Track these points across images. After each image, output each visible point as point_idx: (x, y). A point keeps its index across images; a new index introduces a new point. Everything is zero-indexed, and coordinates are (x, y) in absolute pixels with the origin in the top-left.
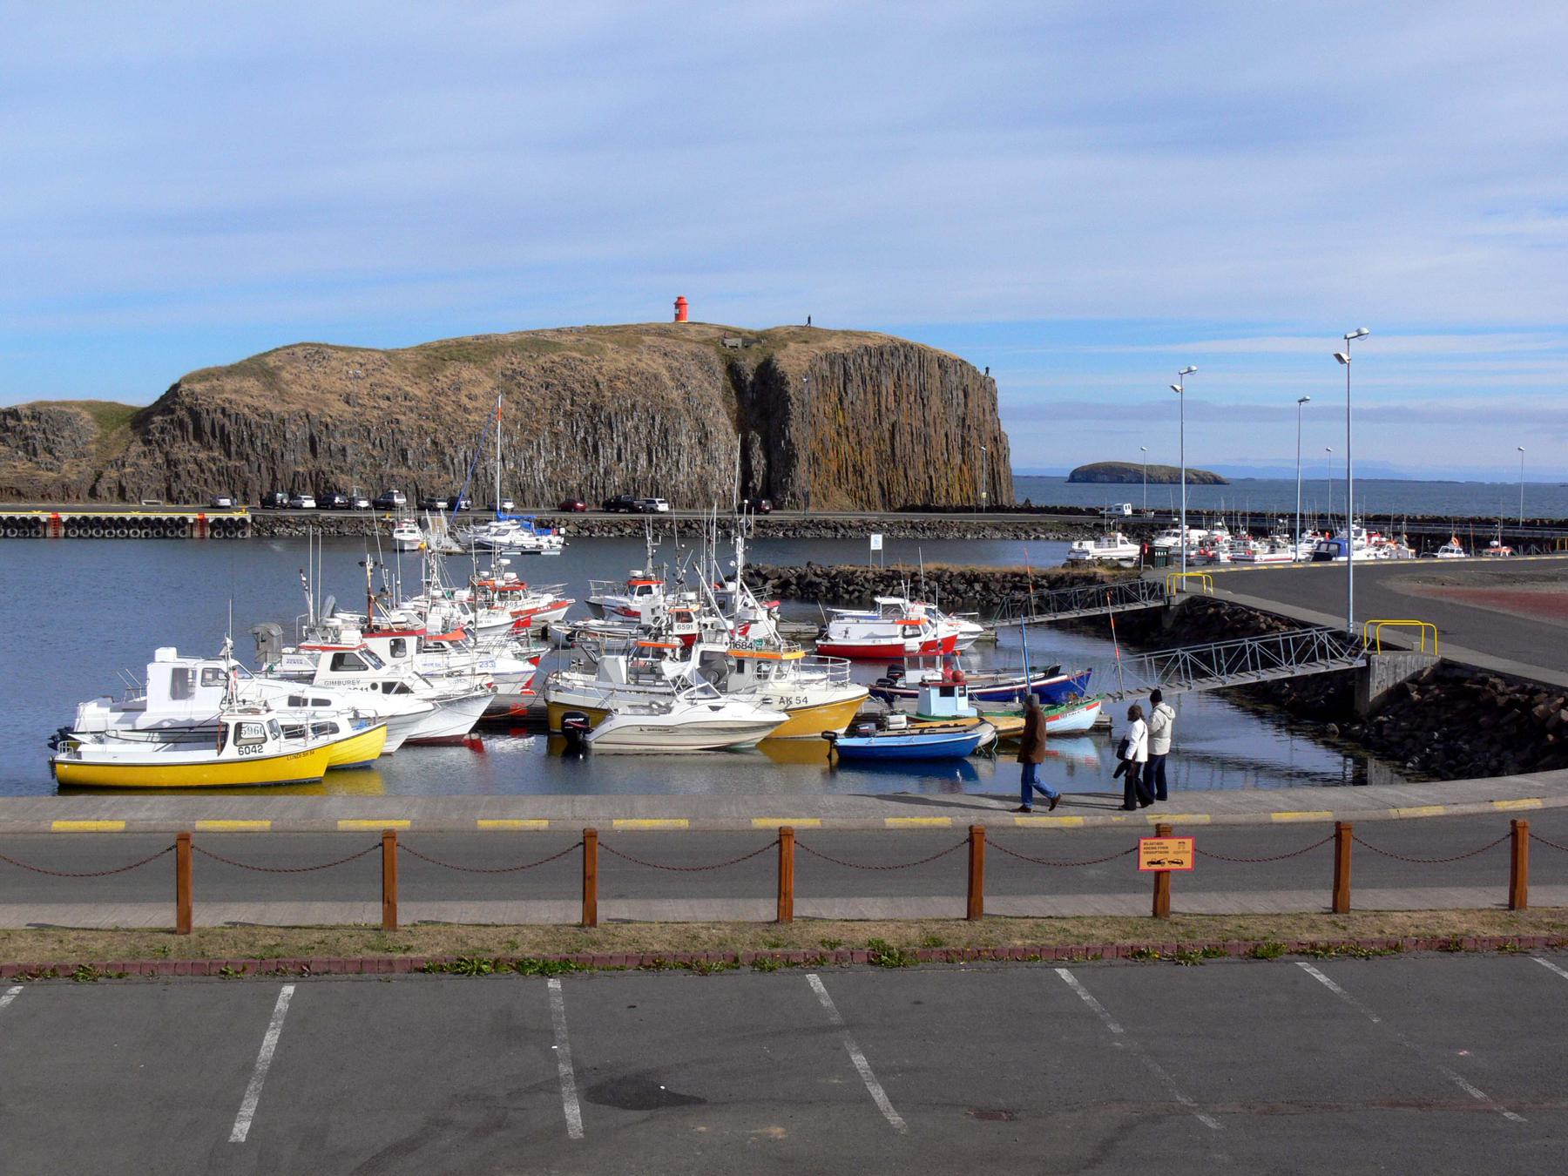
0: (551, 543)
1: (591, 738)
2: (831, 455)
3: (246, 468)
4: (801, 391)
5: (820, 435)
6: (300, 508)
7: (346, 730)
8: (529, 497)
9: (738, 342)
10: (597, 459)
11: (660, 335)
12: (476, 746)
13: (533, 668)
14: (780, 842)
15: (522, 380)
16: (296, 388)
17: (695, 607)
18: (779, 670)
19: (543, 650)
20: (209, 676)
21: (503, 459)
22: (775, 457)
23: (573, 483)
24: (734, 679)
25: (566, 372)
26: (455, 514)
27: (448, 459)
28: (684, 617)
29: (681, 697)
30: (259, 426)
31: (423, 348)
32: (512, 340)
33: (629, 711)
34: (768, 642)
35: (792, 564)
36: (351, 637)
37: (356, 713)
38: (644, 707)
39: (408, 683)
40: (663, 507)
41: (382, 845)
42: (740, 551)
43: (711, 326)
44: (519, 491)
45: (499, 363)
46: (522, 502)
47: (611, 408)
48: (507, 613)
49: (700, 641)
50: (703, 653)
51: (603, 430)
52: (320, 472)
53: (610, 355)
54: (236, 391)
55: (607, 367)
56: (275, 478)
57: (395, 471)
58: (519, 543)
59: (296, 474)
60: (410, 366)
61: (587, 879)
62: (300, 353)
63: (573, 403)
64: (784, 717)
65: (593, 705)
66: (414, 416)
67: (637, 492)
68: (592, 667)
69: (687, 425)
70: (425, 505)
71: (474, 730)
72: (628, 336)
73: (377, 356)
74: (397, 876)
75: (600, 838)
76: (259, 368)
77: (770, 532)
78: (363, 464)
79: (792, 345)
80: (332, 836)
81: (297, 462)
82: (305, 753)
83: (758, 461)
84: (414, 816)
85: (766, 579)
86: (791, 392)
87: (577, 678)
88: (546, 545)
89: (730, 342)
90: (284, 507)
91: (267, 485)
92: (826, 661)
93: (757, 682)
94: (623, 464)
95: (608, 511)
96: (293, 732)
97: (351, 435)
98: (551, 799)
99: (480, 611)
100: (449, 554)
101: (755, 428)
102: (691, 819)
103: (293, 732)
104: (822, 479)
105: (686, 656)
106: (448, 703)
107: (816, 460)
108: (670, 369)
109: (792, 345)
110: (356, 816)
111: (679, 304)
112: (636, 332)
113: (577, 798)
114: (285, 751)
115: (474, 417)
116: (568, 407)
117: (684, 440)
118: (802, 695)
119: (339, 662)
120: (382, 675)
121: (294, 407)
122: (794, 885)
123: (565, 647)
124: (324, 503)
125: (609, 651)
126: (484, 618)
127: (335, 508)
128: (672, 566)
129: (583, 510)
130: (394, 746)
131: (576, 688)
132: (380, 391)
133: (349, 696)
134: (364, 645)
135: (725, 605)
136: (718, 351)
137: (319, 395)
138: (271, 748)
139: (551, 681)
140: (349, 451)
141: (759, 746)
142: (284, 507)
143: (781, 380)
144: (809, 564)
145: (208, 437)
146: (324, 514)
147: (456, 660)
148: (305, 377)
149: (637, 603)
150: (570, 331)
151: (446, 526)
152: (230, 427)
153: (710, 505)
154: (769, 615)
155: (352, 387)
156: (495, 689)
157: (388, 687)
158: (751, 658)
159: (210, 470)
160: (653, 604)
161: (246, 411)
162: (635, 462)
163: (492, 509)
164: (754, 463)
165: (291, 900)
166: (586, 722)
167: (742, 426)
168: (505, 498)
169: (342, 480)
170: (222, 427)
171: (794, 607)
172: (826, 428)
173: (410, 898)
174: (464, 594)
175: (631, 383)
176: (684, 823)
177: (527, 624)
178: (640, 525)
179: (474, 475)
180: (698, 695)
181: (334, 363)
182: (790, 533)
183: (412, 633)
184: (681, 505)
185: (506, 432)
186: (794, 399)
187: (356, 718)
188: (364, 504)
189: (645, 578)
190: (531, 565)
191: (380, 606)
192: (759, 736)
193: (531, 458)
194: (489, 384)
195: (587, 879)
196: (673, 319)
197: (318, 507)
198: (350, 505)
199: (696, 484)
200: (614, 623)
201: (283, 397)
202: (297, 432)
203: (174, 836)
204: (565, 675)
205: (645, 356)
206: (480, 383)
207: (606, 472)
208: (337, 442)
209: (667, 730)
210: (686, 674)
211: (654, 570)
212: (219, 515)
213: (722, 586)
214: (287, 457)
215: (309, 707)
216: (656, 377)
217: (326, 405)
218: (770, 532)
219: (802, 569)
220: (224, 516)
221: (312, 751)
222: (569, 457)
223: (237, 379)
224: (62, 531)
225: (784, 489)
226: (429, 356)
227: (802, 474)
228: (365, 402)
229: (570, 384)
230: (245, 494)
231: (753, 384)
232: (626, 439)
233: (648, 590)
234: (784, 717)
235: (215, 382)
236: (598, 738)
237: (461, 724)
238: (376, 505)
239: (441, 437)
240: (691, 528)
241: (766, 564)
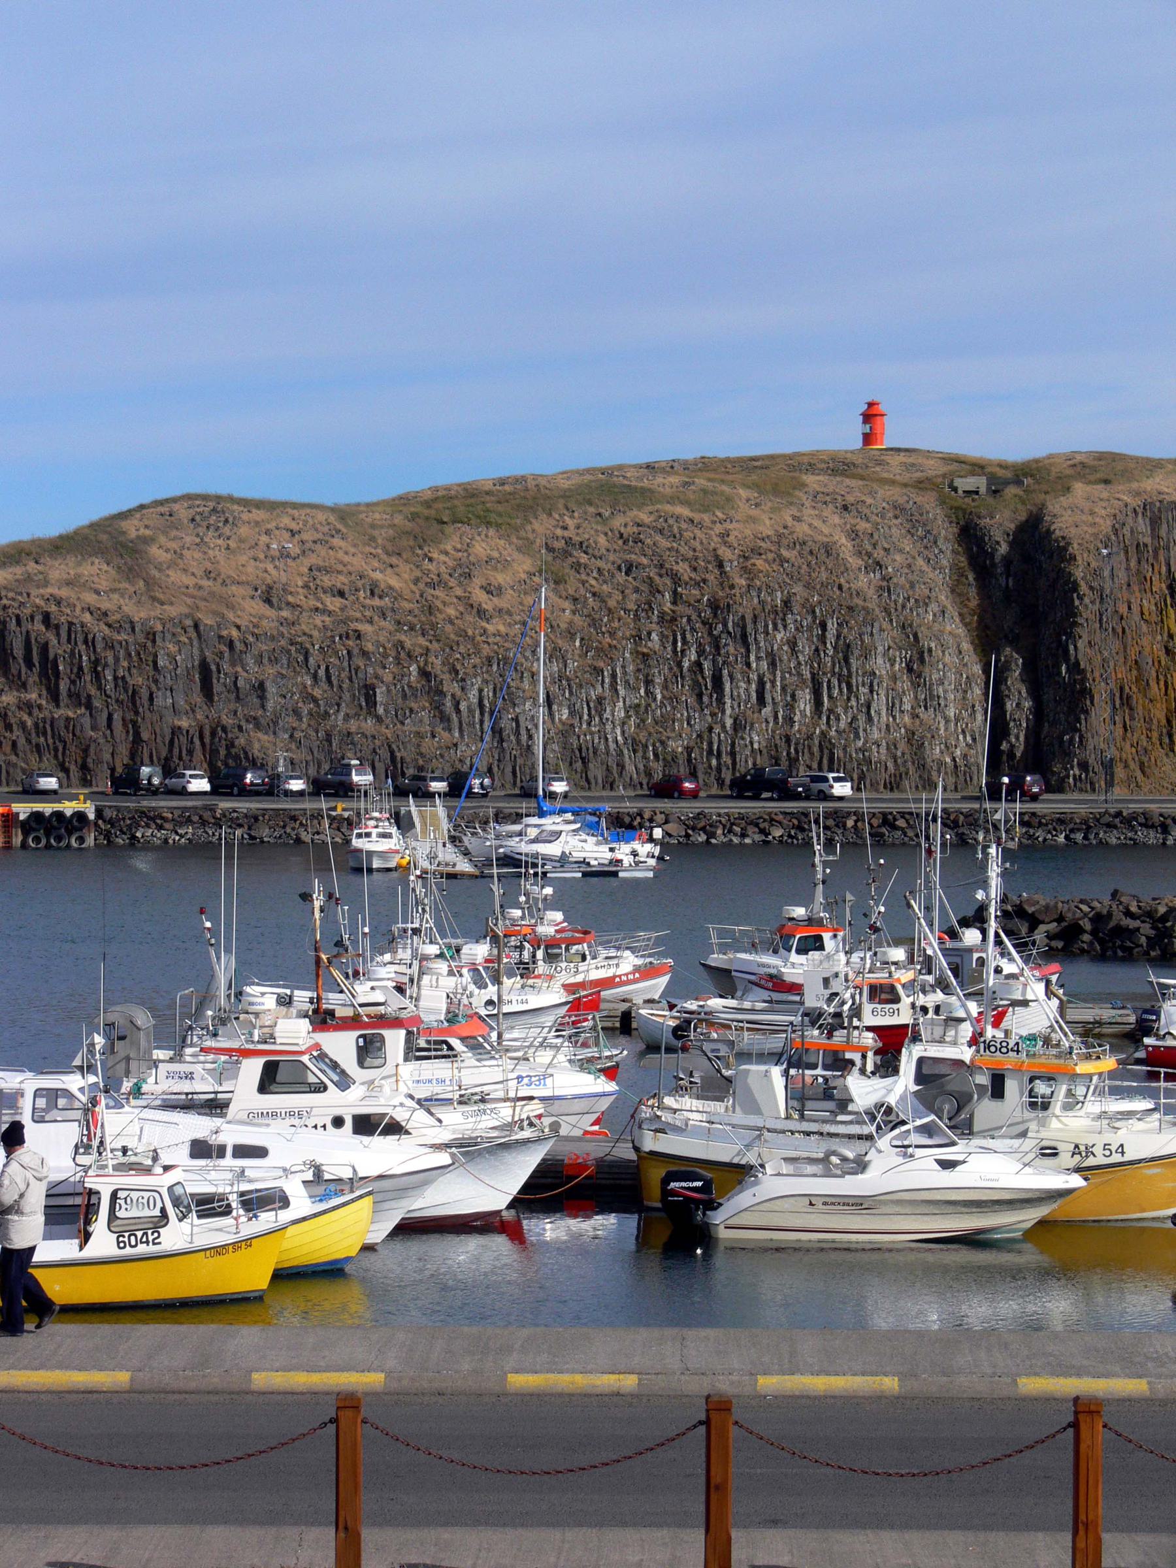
0: (637, 855)
1: (718, 1218)
2: (1155, 690)
3: (87, 721)
4: (1097, 573)
5: (1133, 654)
6: (183, 792)
7: (301, 1203)
8: (596, 771)
9: (979, 483)
10: (721, 701)
11: (834, 472)
12: (514, 1231)
13: (611, 1087)
14: (1075, 1425)
15: (584, 559)
16: (175, 577)
17: (905, 976)
18: (1070, 1094)
19: (617, 1052)
20: (41, 1103)
21: (549, 702)
22: (1049, 695)
23: (677, 746)
24: (985, 1111)
25: (664, 543)
26: (462, 802)
27: (448, 703)
28: (885, 994)
29: (884, 1142)
30: (110, 645)
31: (403, 500)
32: (565, 484)
33: (785, 1168)
34: (1047, 1041)
35: (1087, 891)
36: (294, 1032)
37: (318, 1170)
38: (812, 1161)
39: (400, 1116)
40: (842, 789)
41: (335, 1421)
42: (994, 872)
43: (928, 454)
44: (578, 759)
45: (542, 526)
46: (582, 781)
47: (746, 606)
48: (557, 985)
49: (916, 1038)
50: (921, 1061)
51: (731, 648)
52: (218, 728)
53: (744, 510)
54: (69, 583)
55: (740, 531)
56: (137, 739)
57: (353, 725)
58: (578, 855)
59: (176, 731)
60: (381, 535)
61: (715, 1492)
62: (183, 512)
63: (676, 598)
64: (1076, 1181)
65: (725, 1158)
66: (388, 625)
67: (793, 761)
68: (718, 1087)
69: (885, 637)
70: (406, 785)
71: (510, 1206)
72: (776, 476)
73: (321, 516)
74: (362, 1479)
75: (737, 1414)
76: (109, 541)
77: (1040, 834)
78: (296, 713)
79: (1079, 488)
80: (241, 1400)
81: (178, 710)
82: (236, 1246)
83: (1019, 703)
84: (391, 1363)
85: (1034, 922)
86: (1078, 573)
87: (689, 1108)
88: (627, 860)
89: (965, 483)
90: (153, 792)
91: (124, 750)
92: (1154, 1076)
93: (1029, 1114)
94: (767, 711)
95: (740, 797)
96: (209, 1206)
97: (274, 661)
98: (643, 1334)
99: (507, 982)
100: (452, 876)
101: (1014, 642)
102: (903, 1377)
103: (209, 1206)
104: (1139, 736)
105: (888, 1066)
106: (468, 1151)
107: (1126, 701)
108: (854, 534)
109: (1079, 488)
110: (287, 1367)
111: (871, 415)
112: (792, 468)
113: (691, 1333)
114: (201, 1241)
115: (496, 626)
116: (668, 606)
117: (880, 665)
118: (1115, 1140)
119: (269, 1080)
120: (351, 1101)
121: (172, 611)
122: (1103, 1507)
123: (670, 1050)
124: (226, 783)
125: (745, 1056)
126: (516, 995)
127: (246, 792)
128: (863, 896)
129: (694, 795)
130: (380, 1232)
131: (691, 1126)
132: (326, 581)
133: (296, 1142)
134: (317, 1046)
135: (964, 972)
136: (942, 502)
137: (217, 588)
138: (178, 1235)
139: (645, 1112)
140: (271, 689)
141: (1029, 1235)
142: (153, 792)
143: (1061, 553)
144: (1115, 894)
145: (18, 665)
146: (225, 804)
147: (475, 1072)
148: (192, 557)
149: (796, 966)
150: (671, 467)
151: (445, 825)
152: (58, 648)
153: (931, 786)
154: (1049, 993)
155: (275, 574)
156: (555, 1127)
157: (365, 1125)
158: (1018, 1070)
159: (23, 725)
160: (824, 969)
161: (87, 617)
162: (790, 707)
163: (528, 793)
164: (1009, 706)
165: (166, 1522)
166: (706, 1188)
167: (987, 641)
168: (552, 773)
169: (258, 742)
170: (44, 648)
171: (1087, 972)
172: (1145, 642)
173: (384, 1521)
174: (480, 951)
175: (783, 561)
176: (890, 1384)
177: (593, 1005)
178: (801, 823)
179: (497, 732)
180: (916, 1139)
181: (244, 531)
182: (1079, 837)
183: (395, 1023)
184: (874, 786)
185: (555, 653)
186: (1083, 588)
187: (319, 1182)
188: (296, 785)
189: (810, 921)
190: (599, 903)
191: (336, 973)
192: (1031, 1216)
193: (600, 700)
194: (523, 565)
195: (715, 1492)
196: (859, 444)
197: (215, 791)
198: (272, 788)
199: (902, 746)
200: (755, 1000)
201: (152, 591)
202: (177, 655)
203: (332, 1400)
204: (669, 1101)
205: (808, 512)
206: (506, 566)
207: (738, 726)
208: (249, 672)
209: (859, 1204)
210: (892, 1100)
211: (828, 906)
212: (38, 807)
213: (953, 935)
214: (159, 701)
215: (229, 1161)
216: (828, 549)
217: (231, 607)
218: (1040, 834)
219: (1103, 903)
220: (47, 808)
221: (248, 1241)
222: (673, 699)
223: (71, 560)
224: (17, 840)
225: (1067, 754)
226: (414, 517)
227: (1100, 726)
228: (300, 599)
229: (670, 563)
230: (84, 767)
231: (1007, 561)
232: (773, 665)
233: (816, 944)
234: (1076, 1181)
235: (32, 567)
236: (732, 1216)
237: (494, 1189)
238: (318, 787)
239: (436, 664)
240: (894, 827)
241: (1037, 898)
